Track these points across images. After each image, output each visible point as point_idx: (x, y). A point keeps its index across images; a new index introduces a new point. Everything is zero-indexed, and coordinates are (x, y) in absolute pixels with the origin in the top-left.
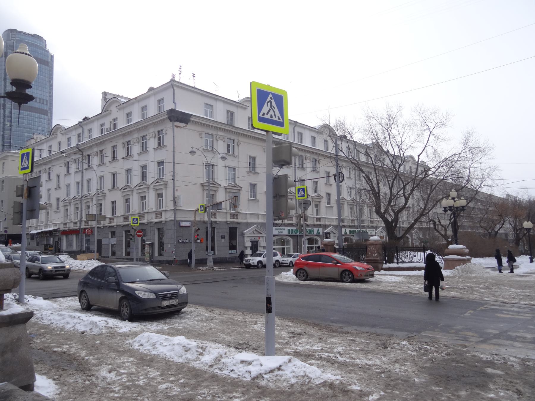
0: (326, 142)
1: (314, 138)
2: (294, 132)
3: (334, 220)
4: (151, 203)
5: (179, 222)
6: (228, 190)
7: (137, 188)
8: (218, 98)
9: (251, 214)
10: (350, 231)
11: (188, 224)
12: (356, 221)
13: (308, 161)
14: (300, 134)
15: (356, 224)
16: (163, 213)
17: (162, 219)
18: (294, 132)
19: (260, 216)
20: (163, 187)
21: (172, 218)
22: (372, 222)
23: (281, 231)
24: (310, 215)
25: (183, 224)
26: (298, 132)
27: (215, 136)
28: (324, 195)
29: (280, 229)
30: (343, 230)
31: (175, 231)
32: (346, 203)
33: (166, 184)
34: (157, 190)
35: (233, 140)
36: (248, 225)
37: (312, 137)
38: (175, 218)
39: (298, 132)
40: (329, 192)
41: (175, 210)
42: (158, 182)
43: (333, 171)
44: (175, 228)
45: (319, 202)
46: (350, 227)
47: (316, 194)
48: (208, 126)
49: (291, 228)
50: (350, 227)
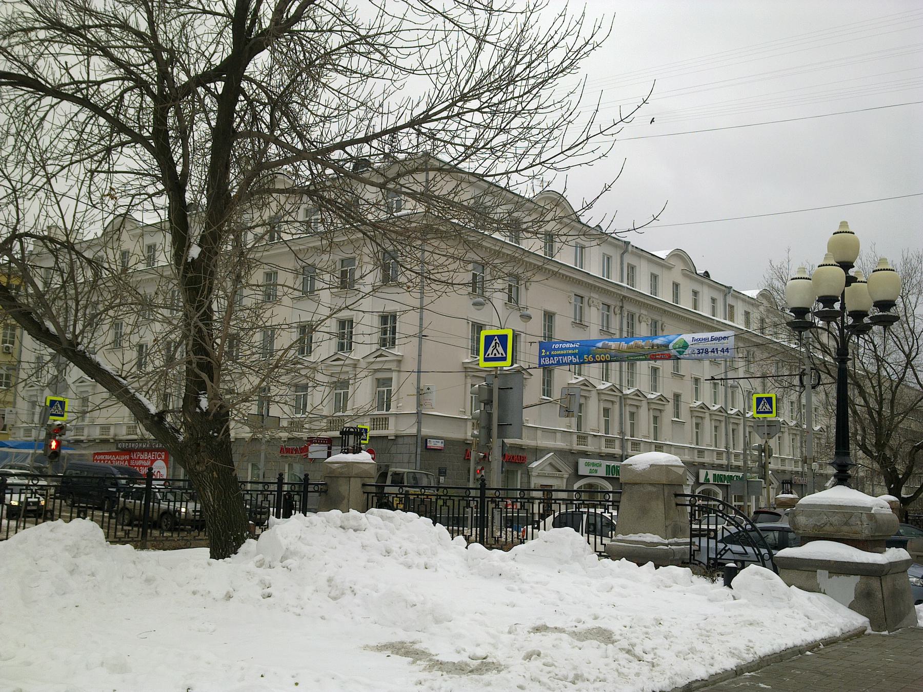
0: (676, 286)
1: (654, 277)
2: (622, 263)
3: (686, 450)
4: (362, 395)
5: (425, 440)
6: (604, 397)
7: (329, 362)
8: (644, 254)
9: (544, 430)
10: (714, 475)
11: (439, 444)
12: (617, 443)
13: (593, 309)
14: (632, 268)
15: (724, 462)
16: (392, 421)
17: (391, 431)
18: (622, 263)
19: (559, 435)
20: (393, 366)
21: (414, 431)
22: (582, 438)
23: (595, 468)
24: (593, 430)
25: (432, 444)
26: (629, 264)
27: (586, 299)
28: (670, 396)
29: (594, 465)
30: (702, 473)
31: (419, 457)
32: (594, 394)
33: (399, 361)
34: (376, 371)
35: (609, 306)
36: (538, 452)
37: (652, 274)
38: (419, 430)
39: (629, 264)
40: (678, 391)
41: (419, 414)
42: (381, 356)
43: (103, 176)
44: (419, 450)
45: (637, 407)
46: (713, 467)
47: (581, 379)
48: (579, 283)
49: (612, 463)
50: (713, 467)
